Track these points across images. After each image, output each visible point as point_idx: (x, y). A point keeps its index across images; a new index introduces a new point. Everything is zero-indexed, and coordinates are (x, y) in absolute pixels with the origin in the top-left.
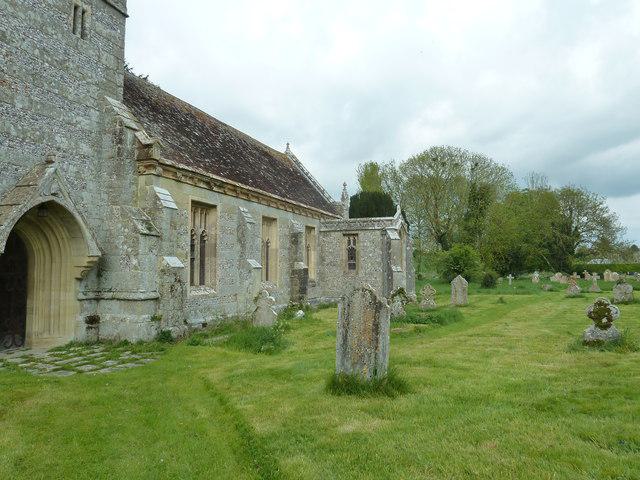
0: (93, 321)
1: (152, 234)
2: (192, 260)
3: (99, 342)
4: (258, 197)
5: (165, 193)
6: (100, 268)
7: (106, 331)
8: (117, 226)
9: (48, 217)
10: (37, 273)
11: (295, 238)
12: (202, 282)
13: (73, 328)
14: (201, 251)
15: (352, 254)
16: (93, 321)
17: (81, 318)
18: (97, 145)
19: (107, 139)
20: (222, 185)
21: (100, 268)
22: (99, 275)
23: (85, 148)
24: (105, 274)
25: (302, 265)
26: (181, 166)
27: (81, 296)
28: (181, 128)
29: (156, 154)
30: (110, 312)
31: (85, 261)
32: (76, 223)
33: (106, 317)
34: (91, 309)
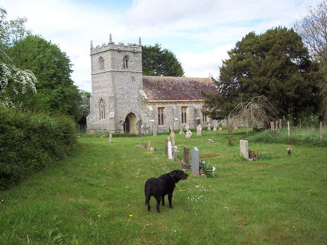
2: (159, 120)
4: (179, 102)
5: (151, 108)
9: (130, 116)
10: (131, 123)
11: (196, 110)
12: (163, 124)
14: (161, 119)
15: (160, 134)
18: (138, 100)
20: (166, 102)
21: (140, 122)
23: (136, 101)
25: (198, 118)
28: (159, 89)
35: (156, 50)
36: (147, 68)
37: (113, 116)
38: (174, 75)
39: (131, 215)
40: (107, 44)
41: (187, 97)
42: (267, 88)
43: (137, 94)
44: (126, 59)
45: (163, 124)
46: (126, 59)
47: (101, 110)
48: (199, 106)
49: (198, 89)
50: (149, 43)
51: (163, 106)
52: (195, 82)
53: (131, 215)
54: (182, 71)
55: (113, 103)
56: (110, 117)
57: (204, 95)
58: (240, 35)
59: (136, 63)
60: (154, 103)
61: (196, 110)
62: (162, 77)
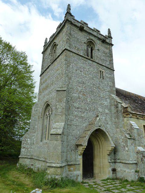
0: (114, 170)
1: (132, 138)
3: (117, 179)
6: (115, 151)
7: (119, 175)
8: (119, 136)
10: (96, 152)
13: (107, 173)
16: (114, 170)
17: (110, 169)
18: (110, 110)
19: (113, 108)
21: (115, 151)
22: (115, 153)
23: (107, 111)
24: (117, 153)
26: (138, 113)
27: (110, 161)
29: (129, 110)
30: (120, 168)
31: (110, 148)
32: (106, 135)
33: (118, 169)
34: (113, 166)
37: (60, 131)
43: (108, 100)
44: (90, 44)
46: (90, 44)
47: (45, 124)
55: (63, 104)
56: (53, 131)
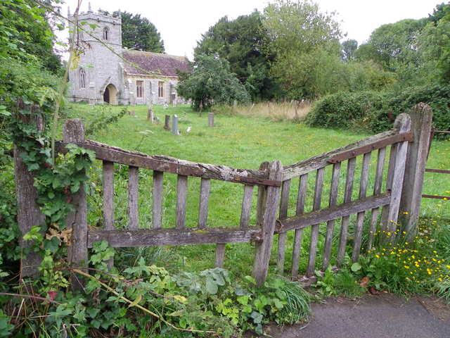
11: (171, 86)
12: (141, 96)
35: (137, 21)
36: (127, 40)
38: (153, 49)
39: (378, 256)
40: (86, 12)
41: (164, 73)
42: (308, 51)
45: (141, 96)
48: (175, 83)
49: (177, 68)
50: (133, 11)
51: (141, 79)
52: (173, 60)
53: (378, 256)
54: (220, 21)
57: (178, 72)
58: (213, 21)
59: (116, 33)
60: (133, 76)
61: (171, 86)
62: (141, 52)
